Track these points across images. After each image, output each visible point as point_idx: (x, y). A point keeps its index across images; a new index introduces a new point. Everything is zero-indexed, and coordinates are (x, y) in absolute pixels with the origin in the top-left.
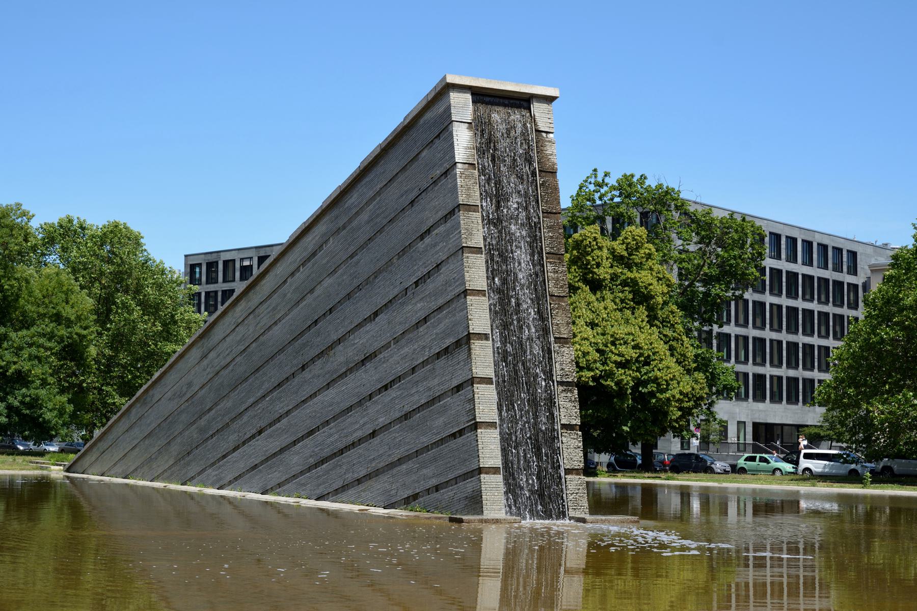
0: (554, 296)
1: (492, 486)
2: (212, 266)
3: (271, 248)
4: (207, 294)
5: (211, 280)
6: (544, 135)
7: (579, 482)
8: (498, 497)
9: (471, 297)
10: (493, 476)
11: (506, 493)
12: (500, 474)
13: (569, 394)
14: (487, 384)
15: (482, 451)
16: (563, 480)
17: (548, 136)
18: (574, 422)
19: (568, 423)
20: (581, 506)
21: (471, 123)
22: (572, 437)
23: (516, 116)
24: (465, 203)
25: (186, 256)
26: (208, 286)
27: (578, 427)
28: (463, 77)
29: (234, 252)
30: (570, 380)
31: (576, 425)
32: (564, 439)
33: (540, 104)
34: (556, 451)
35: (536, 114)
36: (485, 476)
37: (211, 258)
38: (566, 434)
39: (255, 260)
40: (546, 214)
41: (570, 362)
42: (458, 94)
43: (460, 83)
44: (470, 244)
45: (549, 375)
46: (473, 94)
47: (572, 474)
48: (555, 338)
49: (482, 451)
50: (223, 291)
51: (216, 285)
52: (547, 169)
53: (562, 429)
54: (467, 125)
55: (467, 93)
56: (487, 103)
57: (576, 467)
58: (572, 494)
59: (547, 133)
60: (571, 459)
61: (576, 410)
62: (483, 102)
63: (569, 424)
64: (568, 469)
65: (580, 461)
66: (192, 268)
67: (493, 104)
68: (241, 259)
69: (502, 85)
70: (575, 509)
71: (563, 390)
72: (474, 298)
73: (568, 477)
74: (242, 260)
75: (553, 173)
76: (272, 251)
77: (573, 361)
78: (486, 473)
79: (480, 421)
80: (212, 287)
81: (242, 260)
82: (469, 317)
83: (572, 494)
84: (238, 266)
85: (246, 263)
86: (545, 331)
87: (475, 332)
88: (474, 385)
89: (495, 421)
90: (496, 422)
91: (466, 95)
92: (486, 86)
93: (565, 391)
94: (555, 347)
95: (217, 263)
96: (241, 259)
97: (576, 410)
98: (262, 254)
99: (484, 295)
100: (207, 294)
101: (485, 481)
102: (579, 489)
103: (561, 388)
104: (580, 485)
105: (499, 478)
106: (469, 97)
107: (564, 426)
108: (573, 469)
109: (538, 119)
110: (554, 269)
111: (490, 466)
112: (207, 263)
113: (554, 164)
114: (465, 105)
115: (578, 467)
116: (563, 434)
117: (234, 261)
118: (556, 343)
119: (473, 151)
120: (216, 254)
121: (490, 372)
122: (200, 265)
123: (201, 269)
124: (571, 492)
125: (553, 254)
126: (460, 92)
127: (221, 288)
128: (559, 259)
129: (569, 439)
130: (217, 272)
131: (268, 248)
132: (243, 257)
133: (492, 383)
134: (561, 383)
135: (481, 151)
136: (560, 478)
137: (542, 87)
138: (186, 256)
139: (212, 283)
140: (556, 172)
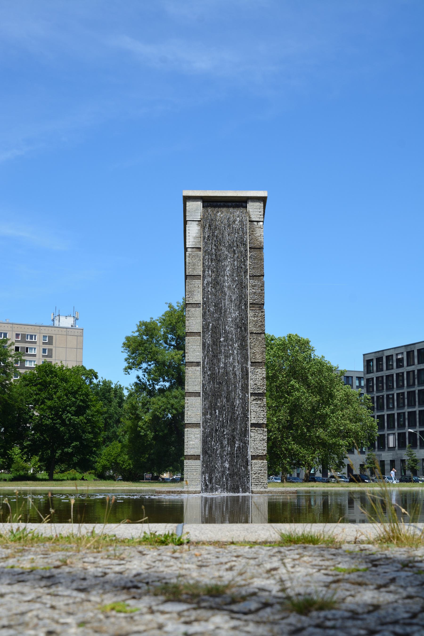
0: (253, 333)
1: (192, 468)
2: (379, 360)
3: (414, 345)
4: (377, 378)
5: (380, 369)
6: (256, 223)
7: (262, 465)
8: (196, 476)
9: (188, 338)
10: (193, 461)
11: (203, 473)
12: (200, 460)
13: (259, 402)
14: (195, 396)
15: (187, 443)
16: (249, 464)
17: (259, 224)
18: (261, 422)
19: (257, 422)
20: (262, 483)
21: (200, 221)
22: (259, 432)
23: (237, 212)
24: (190, 274)
25: (364, 355)
26: (378, 373)
27: (264, 425)
28: (195, 191)
29: (392, 350)
30: (261, 392)
31: (263, 424)
32: (252, 434)
33: (254, 203)
34: (245, 444)
35: (250, 210)
36: (188, 461)
37: (379, 355)
38: (254, 431)
39: (405, 354)
40: (252, 277)
41: (261, 379)
42: (193, 203)
43: (192, 195)
44: (191, 302)
45: (245, 388)
46: (203, 202)
47: (257, 459)
48: (252, 362)
49: (187, 443)
50: (386, 376)
51: (382, 372)
52: (256, 246)
53: (251, 427)
54: (197, 222)
55: (199, 201)
56: (215, 207)
57: (260, 454)
58: (255, 474)
59: (258, 222)
60: (257, 448)
61: (264, 413)
62: (212, 206)
63: (257, 423)
64: (254, 456)
65: (264, 450)
66: (368, 363)
67: (220, 207)
68: (396, 354)
69: (224, 193)
70: (257, 485)
71: (254, 399)
72: (191, 338)
73: (254, 461)
74: (397, 355)
75: (261, 248)
76: (415, 348)
77: (264, 378)
78: (189, 459)
79: (188, 422)
80: (380, 374)
81: (397, 355)
82: (186, 351)
83: (255, 474)
84: (394, 359)
85: (400, 357)
86: (245, 358)
87: (189, 361)
88: (185, 398)
89: (199, 422)
90: (200, 423)
91: (198, 202)
92: (218, 195)
93: (255, 400)
94: (250, 368)
95: (382, 357)
96: (396, 354)
97: (264, 413)
98: (409, 350)
99: (200, 336)
100: (377, 378)
101: (187, 465)
102: (261, 470)
103: (253, 397)
104: (262, 467)
105: (199, 463)
106: (200, 204)
107: (253, 425)
108: (258, 456)
109: (251, 213)
110: (255, 314)
111: (192, 454)
112: (376, 359)
113: (261, 243)
114: (197, 209)
115: (262, 454)
116: (252, 430)
117: (392, 355)
118: (251, 366)
119: (200, 239)
120: (381, 352)
121: (198, 388)
122: (372, 360)
123: (373, 363)
124: (255, 472)
125: (255, 304)
126: (194, 201)
127: (386, 374)
128: (260, 307)
129: (256, 434)
130: (382, 364)
131: (412, 346)
132: (397, 352)
133: (200, 396)
134: (252, 394)
135: (206, 240)
136: (247, 461)
137: (254, 191)
138: (364, 355)
139: (380, 371)
140: (262, 248)
